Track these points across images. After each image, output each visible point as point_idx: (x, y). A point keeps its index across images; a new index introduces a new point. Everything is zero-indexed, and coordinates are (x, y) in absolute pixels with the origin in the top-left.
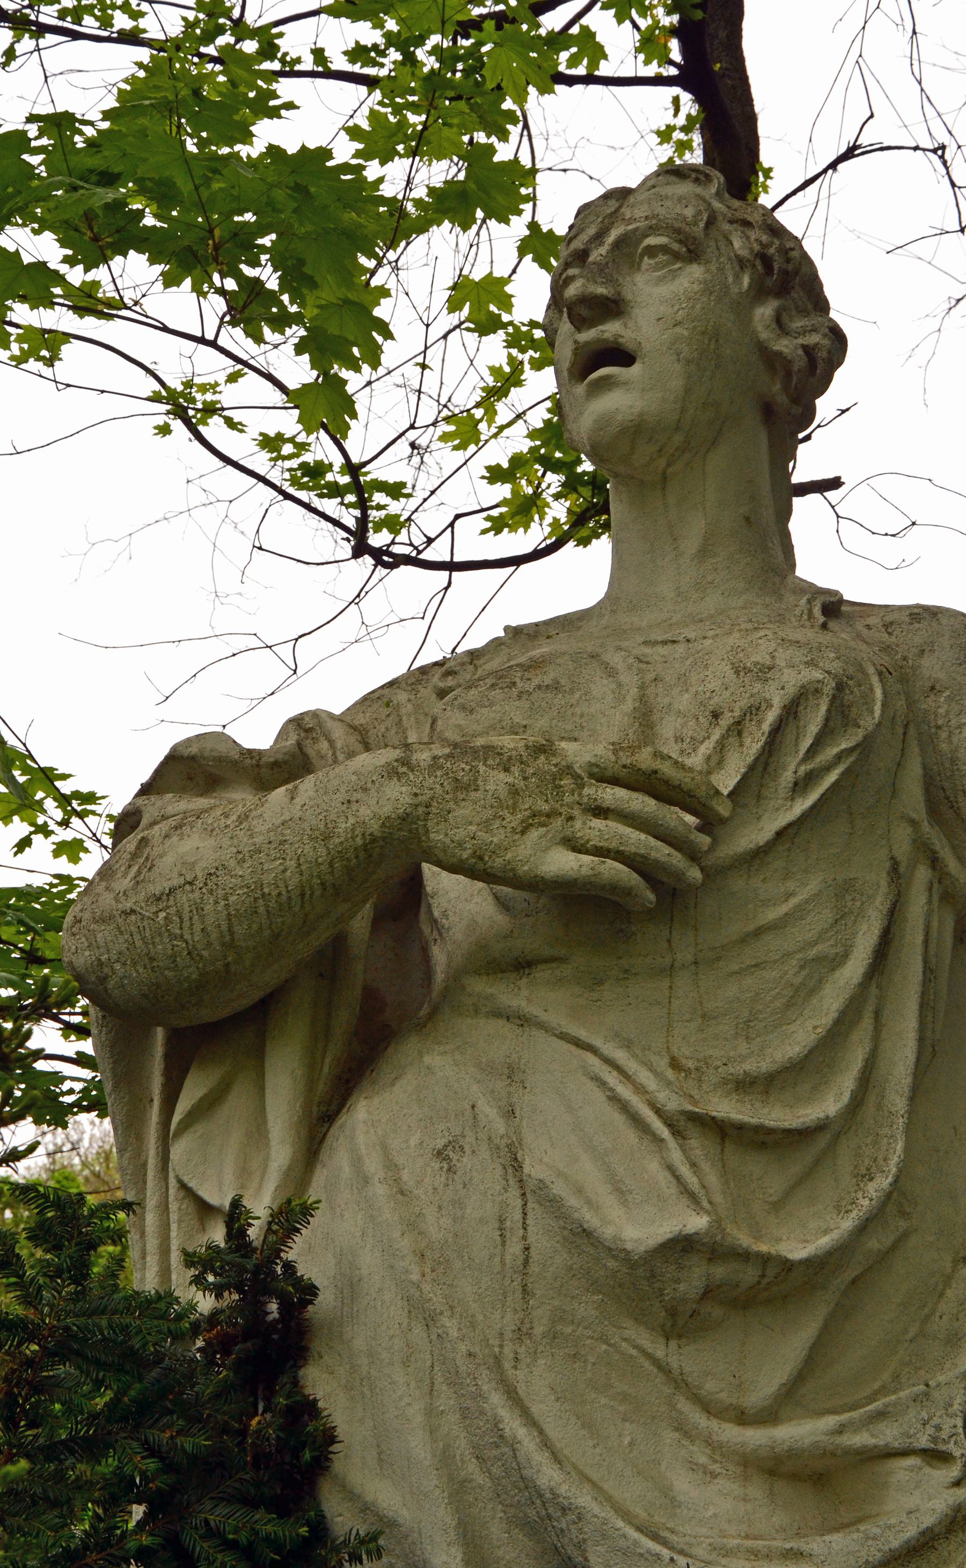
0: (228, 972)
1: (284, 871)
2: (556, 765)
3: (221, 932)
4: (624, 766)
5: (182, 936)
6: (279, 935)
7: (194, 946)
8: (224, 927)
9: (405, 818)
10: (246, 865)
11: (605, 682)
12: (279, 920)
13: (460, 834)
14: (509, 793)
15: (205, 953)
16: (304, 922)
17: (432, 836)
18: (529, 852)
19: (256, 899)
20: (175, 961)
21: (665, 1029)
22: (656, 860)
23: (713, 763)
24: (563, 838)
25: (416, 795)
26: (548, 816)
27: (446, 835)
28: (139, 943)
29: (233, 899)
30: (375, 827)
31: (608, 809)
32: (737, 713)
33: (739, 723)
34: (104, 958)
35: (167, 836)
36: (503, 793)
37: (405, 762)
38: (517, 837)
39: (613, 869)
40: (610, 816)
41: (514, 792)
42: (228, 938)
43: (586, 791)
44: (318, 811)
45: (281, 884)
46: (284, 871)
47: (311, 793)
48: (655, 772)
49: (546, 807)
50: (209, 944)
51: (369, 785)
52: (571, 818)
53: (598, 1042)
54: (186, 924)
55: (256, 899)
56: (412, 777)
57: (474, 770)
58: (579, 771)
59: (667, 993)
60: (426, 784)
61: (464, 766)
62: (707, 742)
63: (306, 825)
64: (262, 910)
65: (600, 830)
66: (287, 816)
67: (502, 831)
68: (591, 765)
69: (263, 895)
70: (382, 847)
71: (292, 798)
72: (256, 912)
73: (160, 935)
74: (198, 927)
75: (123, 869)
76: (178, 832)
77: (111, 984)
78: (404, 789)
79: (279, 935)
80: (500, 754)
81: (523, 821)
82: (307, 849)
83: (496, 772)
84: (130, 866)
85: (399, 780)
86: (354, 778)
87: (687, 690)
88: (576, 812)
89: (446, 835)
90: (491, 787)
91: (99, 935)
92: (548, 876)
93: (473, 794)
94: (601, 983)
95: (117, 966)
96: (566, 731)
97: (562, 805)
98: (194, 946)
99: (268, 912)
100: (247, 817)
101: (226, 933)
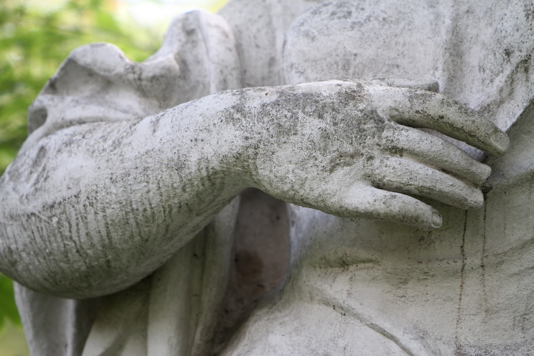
0: (109, 266)
1: (148, 192)
2: (361, 111)
3: (101, 236)
4: (417, 112)
5: (71, 238)
6: (147, 240)
7: (81, 246)
8: (104, 233)
9: (238, 157)
10: (118, 185)
11: (426, 12)
12: (146, 229)
13: (281, 172)
14: (322, 137)
15: (90, 252)
16: (167, 230)
17: (260, 171)
18: (337, 187)
19: (127, 213)
20: (66, 256)
21: (455, 322)
22: (440, 191)
23: (505, 94)
24: (365, 175)
25: (247, 138)
26: (352, 157)
27: (271, 171)
28: (38, 240)
29: (109, 211)
30: (215, 164)
31: (402, 149)
32: (524, 54)
33: (526, 61)
34: (13, 247)
35: (59, 151)
36: (316, 136)
37: (239, 109)
38: (326, 174)
39: (402, 203)
40: (404, 154)
41: (326, 136)
42: (107, 241)
43: (385, 134)
44: (173, 145)
45: (146, 202)
46: (148, 192)
47: (168, 128)
48: (442, 117)
49: (350, 149)
50: (92, 246)
51: (212, 127)
52: (371, 158)
53: (398, 334)
54: (74, 229)
55: (127, 213)
56: (244, 122)
57: (294, 116)
58: (381, 115)
59: (458, 290)
60: (255, 129)
61: (286, 113)
62: (501, 74)
63: (163, 156)
64: (132, 221)
65: (394, 168)
66: (149, 147)
67: (314, 169)
68: (391, 109)
69: (132, 210)
70: (223, 178)
71: (154, 131)
72: (128, 223)
73: (54, 235)
74: (83, 232)
75: (26, 173)
76: (68, 148)
77: (20, 267)
78: (238, 133)
79: (147, 240)
80: (317, 102)
81: (332, 161)
82: (165, 175)
83: (312, 118)
84: (31, 173)
85: (234, 125)
86: (201, 119)
87: (491, 24)
88: (376, 153)
89: (271, 171)
90: (307, 131)
91: (9, 229)
92: (350, 208)
93: (292, 137)
94: (405, 282)
95: (24, 255)
96: (389, 59)
97: (363, 147)
98: (81, 246)
99: (137, 224)
100: (120, 143)
101: (105, 238)
